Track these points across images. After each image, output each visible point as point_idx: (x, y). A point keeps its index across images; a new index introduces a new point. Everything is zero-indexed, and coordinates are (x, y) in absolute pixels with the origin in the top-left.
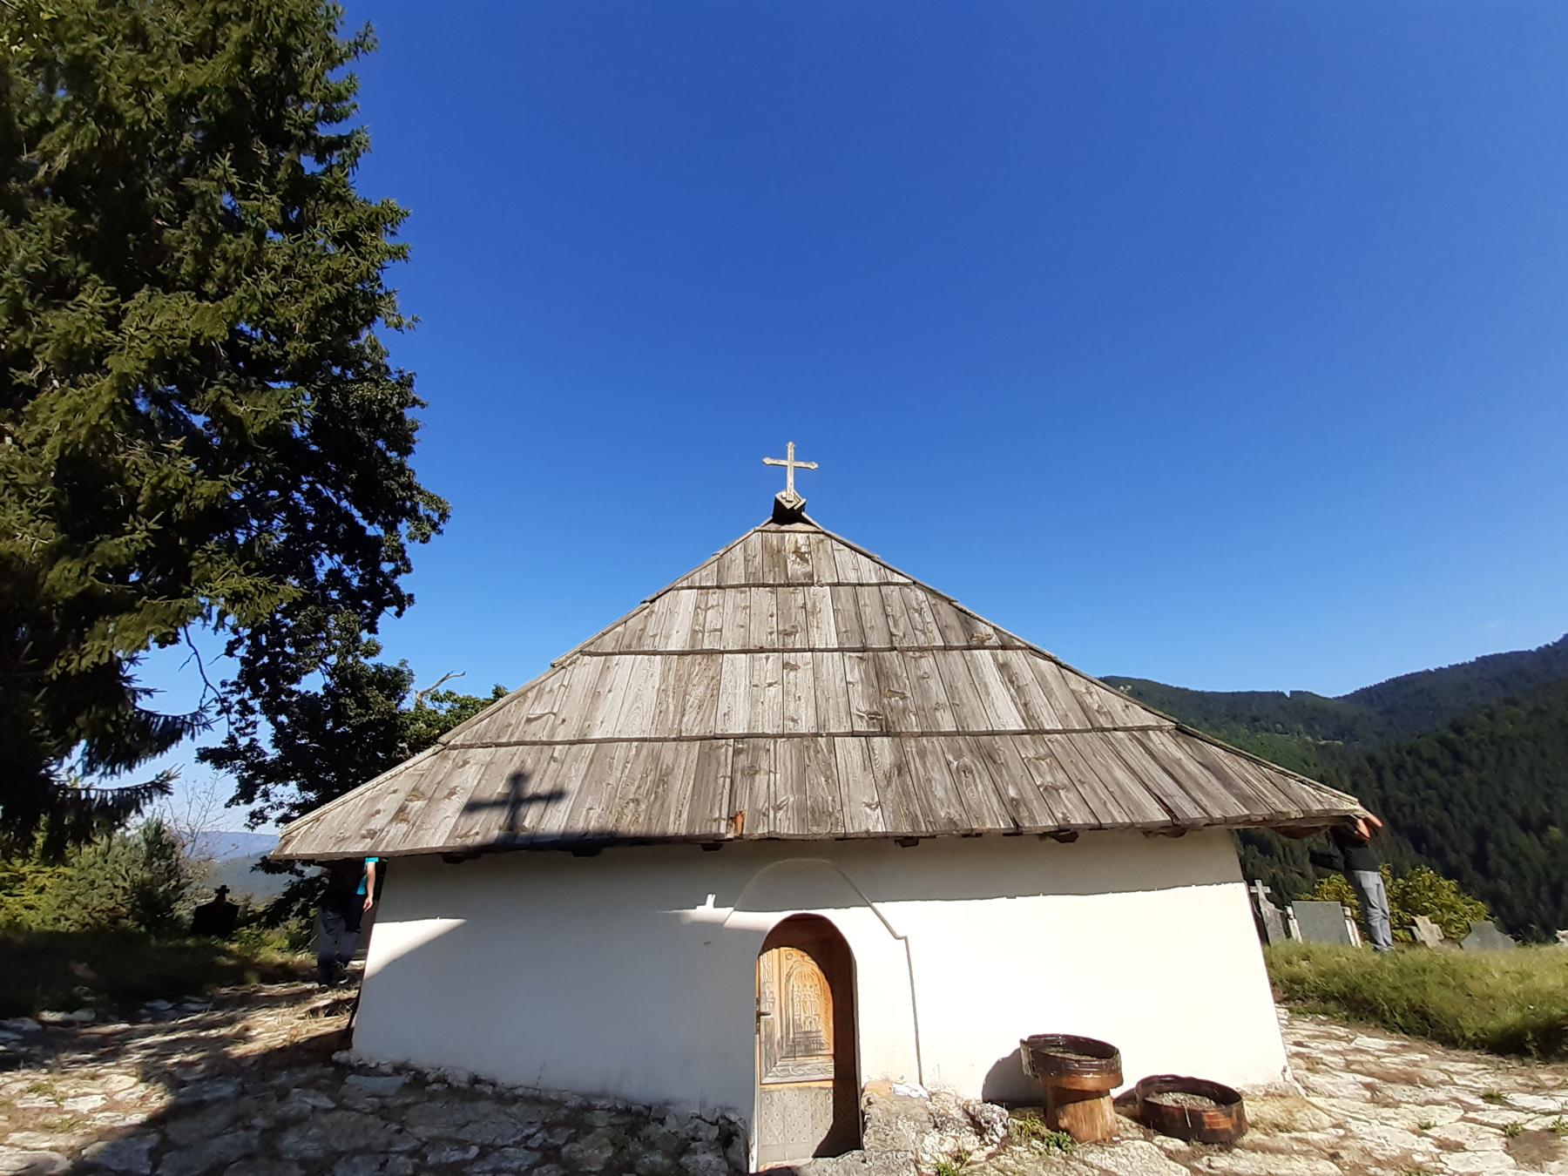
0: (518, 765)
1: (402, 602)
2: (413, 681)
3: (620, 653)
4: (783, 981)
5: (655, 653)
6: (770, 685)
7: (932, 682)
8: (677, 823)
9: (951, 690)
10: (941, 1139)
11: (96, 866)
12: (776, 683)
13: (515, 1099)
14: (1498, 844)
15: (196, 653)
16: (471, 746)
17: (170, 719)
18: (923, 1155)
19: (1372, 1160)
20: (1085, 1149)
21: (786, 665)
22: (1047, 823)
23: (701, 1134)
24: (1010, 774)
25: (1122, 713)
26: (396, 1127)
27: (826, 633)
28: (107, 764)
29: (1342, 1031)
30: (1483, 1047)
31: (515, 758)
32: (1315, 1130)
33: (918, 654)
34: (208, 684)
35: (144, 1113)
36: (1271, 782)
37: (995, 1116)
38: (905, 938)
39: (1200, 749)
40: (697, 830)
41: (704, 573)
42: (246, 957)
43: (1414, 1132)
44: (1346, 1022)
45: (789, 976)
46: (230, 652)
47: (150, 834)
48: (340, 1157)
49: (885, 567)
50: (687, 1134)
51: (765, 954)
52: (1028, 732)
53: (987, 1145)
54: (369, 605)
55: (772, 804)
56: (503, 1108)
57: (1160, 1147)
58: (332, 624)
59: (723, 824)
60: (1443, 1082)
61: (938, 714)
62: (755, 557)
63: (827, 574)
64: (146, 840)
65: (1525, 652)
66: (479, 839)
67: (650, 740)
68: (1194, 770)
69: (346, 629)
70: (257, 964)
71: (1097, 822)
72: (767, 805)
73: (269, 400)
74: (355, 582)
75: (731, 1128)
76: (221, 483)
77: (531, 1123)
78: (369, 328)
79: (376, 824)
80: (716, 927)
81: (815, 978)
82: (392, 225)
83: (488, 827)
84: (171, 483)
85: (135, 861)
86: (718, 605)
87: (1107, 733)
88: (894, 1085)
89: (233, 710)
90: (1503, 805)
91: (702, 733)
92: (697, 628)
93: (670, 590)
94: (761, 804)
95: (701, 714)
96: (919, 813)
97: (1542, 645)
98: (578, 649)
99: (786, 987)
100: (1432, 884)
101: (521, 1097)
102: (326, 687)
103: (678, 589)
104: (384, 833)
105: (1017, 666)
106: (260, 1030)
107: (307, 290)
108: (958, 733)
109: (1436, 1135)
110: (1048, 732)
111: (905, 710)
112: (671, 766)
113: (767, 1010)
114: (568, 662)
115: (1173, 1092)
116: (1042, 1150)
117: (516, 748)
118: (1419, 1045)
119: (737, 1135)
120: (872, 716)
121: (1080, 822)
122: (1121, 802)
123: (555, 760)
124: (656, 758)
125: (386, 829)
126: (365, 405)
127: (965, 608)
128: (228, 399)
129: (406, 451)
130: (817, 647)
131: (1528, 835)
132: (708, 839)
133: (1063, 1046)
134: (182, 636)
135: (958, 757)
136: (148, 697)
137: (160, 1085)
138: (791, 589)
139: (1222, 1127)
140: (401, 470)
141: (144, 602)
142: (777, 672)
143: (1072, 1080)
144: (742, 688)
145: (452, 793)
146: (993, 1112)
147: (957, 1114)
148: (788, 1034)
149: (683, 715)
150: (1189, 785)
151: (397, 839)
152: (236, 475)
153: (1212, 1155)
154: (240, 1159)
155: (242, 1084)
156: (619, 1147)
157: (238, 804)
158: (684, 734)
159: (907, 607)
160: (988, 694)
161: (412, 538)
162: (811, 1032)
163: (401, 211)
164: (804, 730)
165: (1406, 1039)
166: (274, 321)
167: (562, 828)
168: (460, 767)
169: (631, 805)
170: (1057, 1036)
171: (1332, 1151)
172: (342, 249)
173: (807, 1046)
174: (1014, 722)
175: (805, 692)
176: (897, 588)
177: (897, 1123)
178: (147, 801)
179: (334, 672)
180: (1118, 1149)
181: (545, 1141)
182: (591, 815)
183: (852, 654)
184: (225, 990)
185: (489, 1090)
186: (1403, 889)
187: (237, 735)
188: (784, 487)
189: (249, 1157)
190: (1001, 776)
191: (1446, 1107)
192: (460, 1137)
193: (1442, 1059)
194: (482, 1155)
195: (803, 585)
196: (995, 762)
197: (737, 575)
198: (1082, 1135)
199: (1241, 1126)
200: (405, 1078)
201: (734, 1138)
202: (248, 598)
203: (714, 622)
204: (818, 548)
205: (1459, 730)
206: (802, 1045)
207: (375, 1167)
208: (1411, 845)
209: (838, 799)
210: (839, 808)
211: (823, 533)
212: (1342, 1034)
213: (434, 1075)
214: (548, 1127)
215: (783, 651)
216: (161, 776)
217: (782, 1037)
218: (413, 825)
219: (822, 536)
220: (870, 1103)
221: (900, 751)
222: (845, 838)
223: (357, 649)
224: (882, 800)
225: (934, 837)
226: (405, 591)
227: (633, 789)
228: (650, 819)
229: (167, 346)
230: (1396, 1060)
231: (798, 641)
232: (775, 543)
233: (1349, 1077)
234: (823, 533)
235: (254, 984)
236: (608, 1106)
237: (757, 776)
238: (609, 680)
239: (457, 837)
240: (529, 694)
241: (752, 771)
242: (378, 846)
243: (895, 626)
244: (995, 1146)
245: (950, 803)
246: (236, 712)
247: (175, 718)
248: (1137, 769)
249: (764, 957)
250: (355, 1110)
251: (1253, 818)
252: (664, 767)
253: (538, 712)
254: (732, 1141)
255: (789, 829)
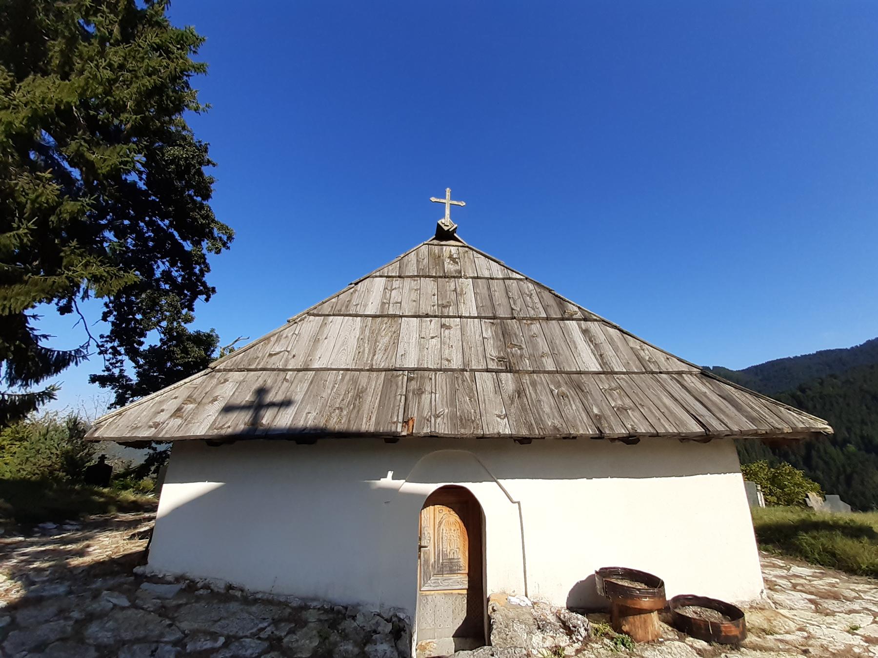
0: (261, 383)
1: (209, 292)
2: (219, 341)
3: (334, 315)
4: (437, 527)
5: (357, 316)
6: (432, 338)
7: (539, 340)
8: (368, 424)
9: (551, 344)
10: (543, 638)
11: (40, 441)
12: (436, 336)
13: (256, 601)
14: (818, 451)
15: (83, 318)
16: (231, 370)
17: (61, 353)
18: (533, 650)
19: (829, 653)
20: (641, 647)
21: (443, 326)
22: (622, 431)
23: (380, 629)
24: (594, 400)
25: (664, 362)
26: (168, 622)
27: (470, 307)
28: (23, 380)
29: (780, 563)
30: (871, 574)
31: (260, 379)
32: (787, 633)
33: (529, 322)
34: (90, 337)
35: (6, 601)
36: (768, 409)
37: (579, 622)
38: (519, 503)
39: (719, 387)
40: (382, 429)
41: (390, 268)
42: (112, 497)
43: (848, 632)
44: (782, 556)
45: (440, 523)
46: (105, 317)
47: (71, 425)
48: (124, 644)
49: (507, 268)
50: (371, 627)
51: (425, 509)
52: (604, 373)
53: (574, 642)
54: (188, 294)
55: (433, 413)
56: (246, 608)
57: (691, 646)
58: (163, 302)
59: (400, 425)
60: (855, 598)
61: (544, 360)
62: (423, 259)
63: (470, 271)
64: (69, 428)
65: (844, 349)
66: (230, 430)
67: (352, 370)
68: (716, 400)
69: (172, 305)
70: (119, 501)
71: (655, 432)
72: (430, 414)
73: (112, 152)
74: (179, 279)
75: (401, 625)
76: (80, 203)
77: (264, 619)
78: (180, 114)
79: (160, 418)
80: (394, 491)
81: (458, 526)
82: (194, 47)
83: (238, 422)
84: (43, 199)
85: (62, 439)
86: (399, 287)
87: (655, 375)
88: (510, 597)
89: (108, 352)
91: (386, 367)
92: (385, 301)
93: (368, 277)
94: (426, 413)
95: (386, 354)
96: (533, 422)
97: (854, 345)
98: (305, 311)
99: (438, 531)
100: (790, 472)
101: (259, 599)
102: (161, 340)
103: (374, 277)
104: (165, 425)
105: (594, 332)
106: (96, 547)
107: (134, 79)
108: (557, 372)
109: (863, 634)
110: (616, 373)
111: (521, 356)
112: (365, 387)
113: (426, 545)
114: (299, 319)
115: (692, 605)
116: (612, 647)
117: (261, 372)
118: (831, 572)
119: (405, 631)
120: (500, 359)
121: (644, 431)
122: (670, 419)
123: (287, 381)
124: (355, 381)
125: (166, 422)
126: (175, 160)
127: (559, 295)
128: (85, 149)
129: (206, 196)
130: (463, 315)
131: (835, 447)
132: (388, 435)
133: (621, 575)
134: (74, 309)
135: (558, 386)
136: (45, 339)
137: (19, 583)
138: (447, 280)
139: (733, 634)
140: (202, 207)
141: (30, 277)
142: (437, 330)
143: (635, 602)
144: (414, 339)
145: (215, 400)
146: (578, 620)
147: (552, 619)
148: (439, 559)
149: (374, 355)
150: (713, 409)
151: (173, 429)
152: (89, 199)
153: (727, 653)
154: (58, 640)
155: (70, 586)
156: (324, 638)
157: (115, 408)
158: (374, 367)
159: (522, 293)
160: (576, 348)
161: (210, 250)
162: (453, 559)
163: (200, 37)
164: (454, 367)
165: (822, 569)
166: (113, 99)
167: (288, 425)
168: (222, 383)
169: (337, 411)
170: (618, 568)
171: (804, 648)
172: (158, 54)
173: (450, 568)
174: (595, 366)
175: (456, 343)
176: (515, 281)
177: (513, 625)
178: (41, 403)
179: (168, 331)
180: (663, 648)
181: (272, 633)
182: (309, 417)
183: (486, 320)
184: (93, 517)
185: (238, 594)
186: (774, 474)
187: (111, 367)
188: (443, 216)
189: (63, 640)
190: (587, 400)
191: (862, 614)
192: (212, 630)
193: (848, 581)
194: (226, 645)
195: (454, 277)
196: (583, 391)
197: (412, 270)
198: (638, 636)
199: (744, 632)
200: (182, 585)
201: (402, 633)
202: (103, 280)
203: (397, 297)
204: (464, 255)
205: (803, 391)
206: (448, 567)
207: (148, 653)
208: (770, 450)
209: (478, 411)
210: (478, 417)
211: (468, 247)
212: (782, 565)
213: (202, 583)
214: (276, 622)
215: (442, 317)
216: (49, 388)
217: (435, 561)
218: (186, 420)
219: (467, 249)
220: (494, 610)
221: (519, 382)
222: (483, 437)
223: (179, 318)
224: (508, 413)
225: (544, 438)
226: (210, 285)
227: (339, 401)
228: (349, 421)
229: (39, 108)
230: (820, 582)
232: (437, 251)
233: (798, 595)
234: (468, 247)
235: (113, 512)
236: (318, 607)
237: (423, 396)
238: (326, 331)
239: (215, 428)
240: (272, 339)
241: (420, 392)
242: (160, 433)
243: (514, 304)
244: (580, 643)
245: (554, 416)
246: (110, 353)
247: (65, 353)
248: (678, 398)
249: (425, 512)
250: (143, 609)
251: (759, 432)
252: (360, 387)
253: (278, 350)
254: (401, 635)
255: (444, 430)
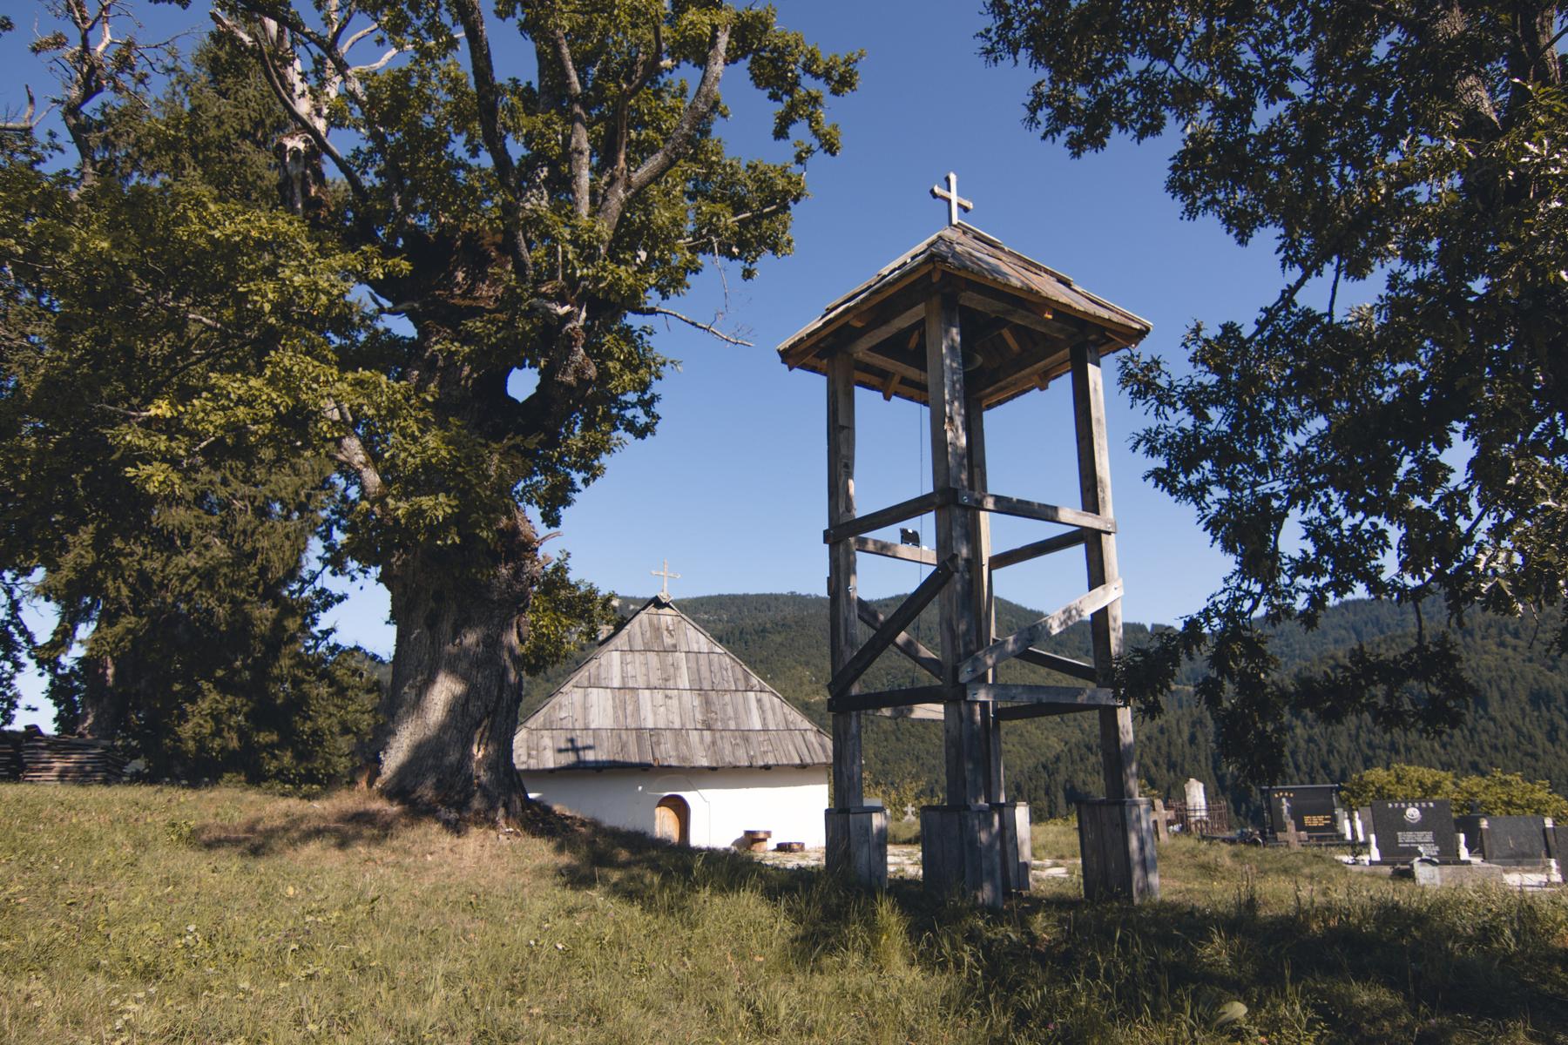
9: (736, 711)
21: (666, 696)
22: (761, 763)
27: (684, 681)
83: (569, 758)
90: (1325, 766)
175: (675, 708)
231: (671, 684)
241: (659, 743)
